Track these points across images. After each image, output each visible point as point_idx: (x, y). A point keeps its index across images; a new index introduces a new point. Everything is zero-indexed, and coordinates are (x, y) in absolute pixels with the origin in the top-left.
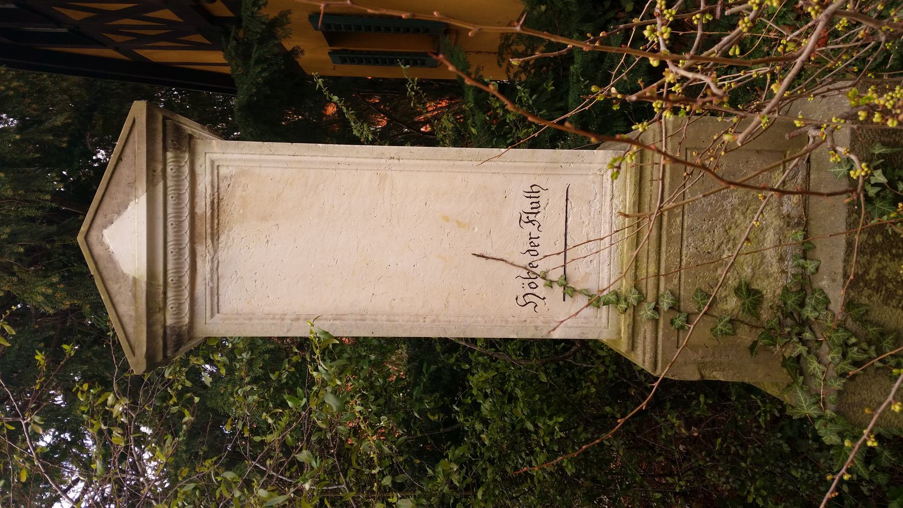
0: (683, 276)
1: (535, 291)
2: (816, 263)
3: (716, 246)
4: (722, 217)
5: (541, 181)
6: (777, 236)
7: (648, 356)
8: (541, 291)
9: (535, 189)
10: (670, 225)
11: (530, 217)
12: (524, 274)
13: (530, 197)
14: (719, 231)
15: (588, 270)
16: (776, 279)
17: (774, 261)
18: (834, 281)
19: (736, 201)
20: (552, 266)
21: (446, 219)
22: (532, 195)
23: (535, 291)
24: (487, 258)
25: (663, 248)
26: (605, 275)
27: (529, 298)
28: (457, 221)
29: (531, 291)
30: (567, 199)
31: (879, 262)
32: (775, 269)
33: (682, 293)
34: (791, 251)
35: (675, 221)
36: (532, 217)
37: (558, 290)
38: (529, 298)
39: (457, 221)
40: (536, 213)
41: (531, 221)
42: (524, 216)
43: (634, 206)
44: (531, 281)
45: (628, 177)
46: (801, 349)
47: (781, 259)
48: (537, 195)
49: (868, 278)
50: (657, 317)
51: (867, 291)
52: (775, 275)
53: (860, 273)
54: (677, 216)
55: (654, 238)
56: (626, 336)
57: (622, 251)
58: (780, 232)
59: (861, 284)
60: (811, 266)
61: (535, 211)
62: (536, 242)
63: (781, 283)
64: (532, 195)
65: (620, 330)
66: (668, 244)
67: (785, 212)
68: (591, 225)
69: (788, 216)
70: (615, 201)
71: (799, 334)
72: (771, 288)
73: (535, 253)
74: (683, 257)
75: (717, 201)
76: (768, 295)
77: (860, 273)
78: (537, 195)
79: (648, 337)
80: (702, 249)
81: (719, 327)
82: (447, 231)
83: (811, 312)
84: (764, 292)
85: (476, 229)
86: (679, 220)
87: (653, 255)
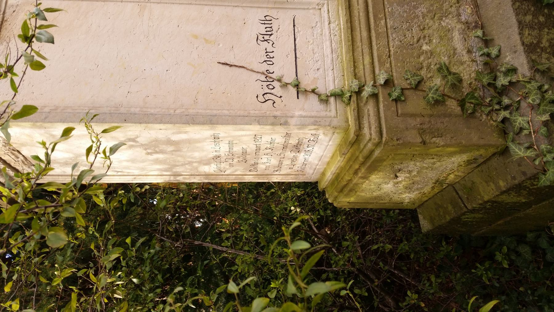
0: (393, 62)
1: (272, 91)
2: (498, 48)
3: (415, 40)
4: (416, 20)
5: (273, 13)
6: (462, 36)
7: (373, 128)
8: (278, 91)
9: (268, 18)
10: (376, 25)
11: (266, 36)
12: (263, 78)
13: (265, 24)
14: (415, 30)
15: (316, 76)
16: (468, 65)
17: (464, 53)
18: (515, 52)
19: (425, 10)
20: (283, 68)
21: (196, 37)
22: (266, 22)
23: (272, 91)
24: (231, 66)
25: (374, 43)
26: (330, 78)
27: (267, 97)
28: (205, 39)
29: (269, 91)
30: (294, 26)
31: (548, 35)
32: (466, 58)
33: (394, 74)
34: (474, 43)
35: (380, 23)
36: (266, 37)
37: (294, 91)
38: (267, 97)
39: (205, 39)
40: (271, 35)
41: (266, 40)
42: (261, 37)
43: (347, 22)
44: (268, 83)
45: (340, 9)
46: (504, 114)
47: (469, 52)
48: (270, 22)
49: (542, 45)
50: (376, 92)
51: (544, 55)
52: (468, 63)
53: (535, 42)
54: (381, 19)
55: (366, 38)
56: (353, 121)
57: (342, 59)
58: (463, 32)
59: (538, 50)
60: (494, 52)
61: (270, 33)
62: (271, 55)
63: (473, 69)
64: (266, 22)
65: (347, 119)
66: (377, 38)
67: (463, 19)
68: (315, 43)
69: (467, 23)
70: (332, 25)
71: (499, 103)
72: (469, 70)
73: (271, 63)
74: (391, 49)
75: (410, 10)
76: (465, 77)
77: (535, 42)
78: (270, 22)
79: (372, 113)
80: (405, 42)
81: (430, 95)
82: (195, 46)
83: (504, 79)
84: (462, 75)
85: (221, 45)
86: (383, 22)
87: (366, 50)
